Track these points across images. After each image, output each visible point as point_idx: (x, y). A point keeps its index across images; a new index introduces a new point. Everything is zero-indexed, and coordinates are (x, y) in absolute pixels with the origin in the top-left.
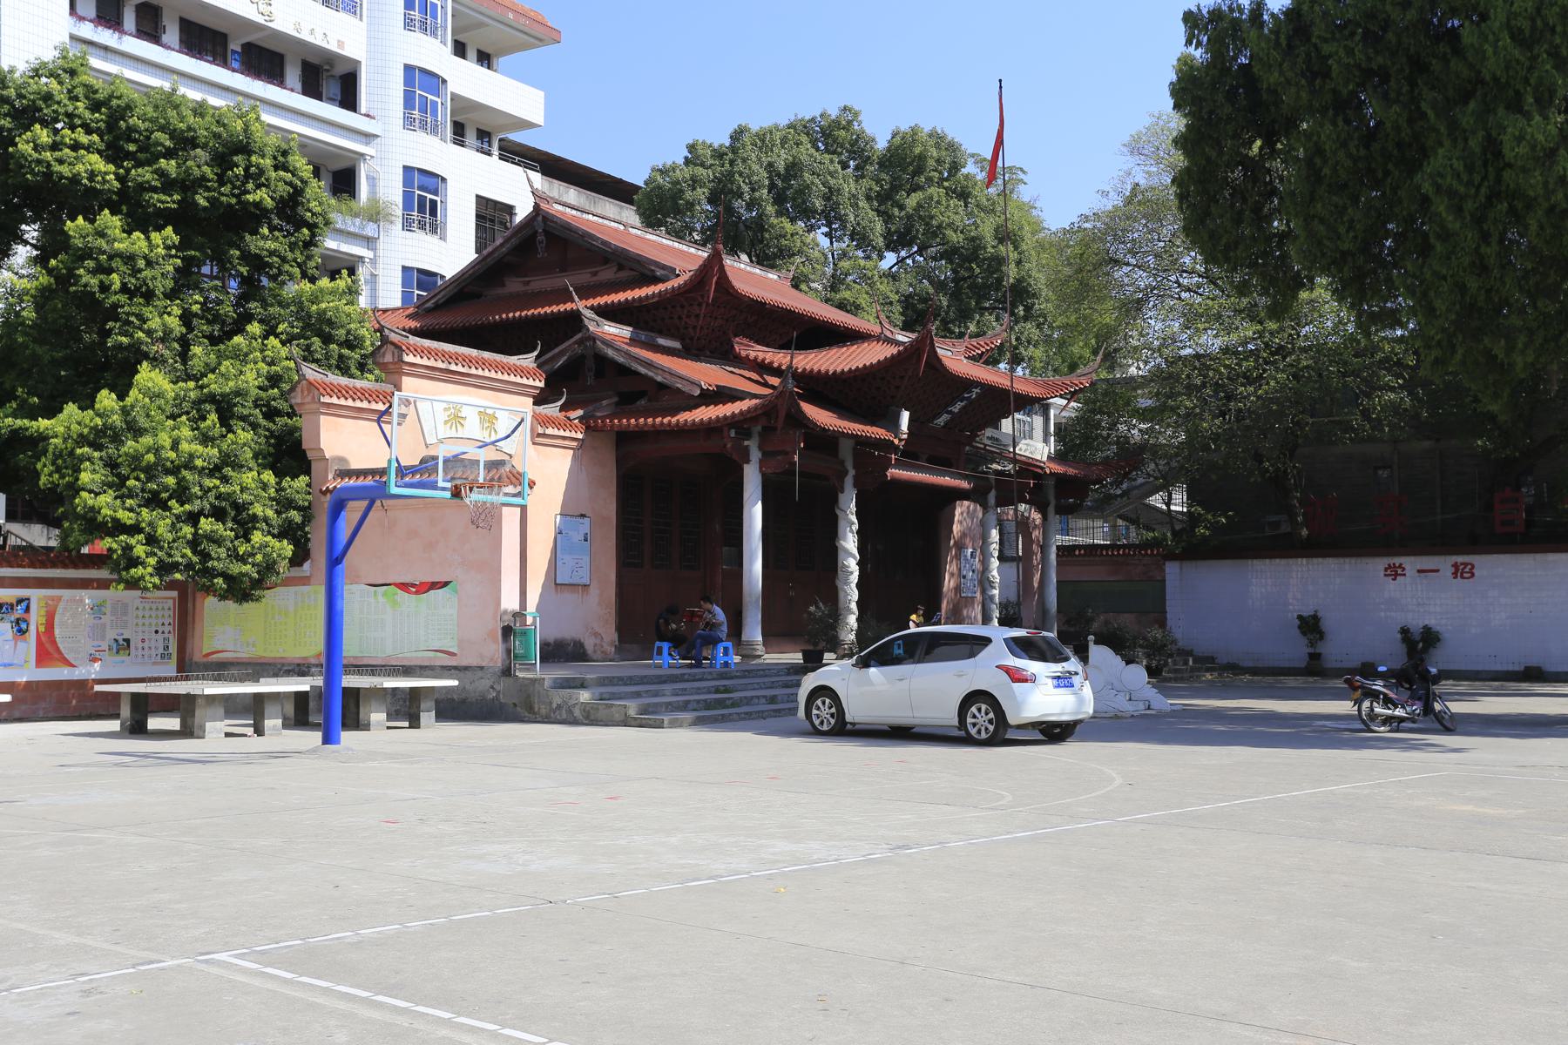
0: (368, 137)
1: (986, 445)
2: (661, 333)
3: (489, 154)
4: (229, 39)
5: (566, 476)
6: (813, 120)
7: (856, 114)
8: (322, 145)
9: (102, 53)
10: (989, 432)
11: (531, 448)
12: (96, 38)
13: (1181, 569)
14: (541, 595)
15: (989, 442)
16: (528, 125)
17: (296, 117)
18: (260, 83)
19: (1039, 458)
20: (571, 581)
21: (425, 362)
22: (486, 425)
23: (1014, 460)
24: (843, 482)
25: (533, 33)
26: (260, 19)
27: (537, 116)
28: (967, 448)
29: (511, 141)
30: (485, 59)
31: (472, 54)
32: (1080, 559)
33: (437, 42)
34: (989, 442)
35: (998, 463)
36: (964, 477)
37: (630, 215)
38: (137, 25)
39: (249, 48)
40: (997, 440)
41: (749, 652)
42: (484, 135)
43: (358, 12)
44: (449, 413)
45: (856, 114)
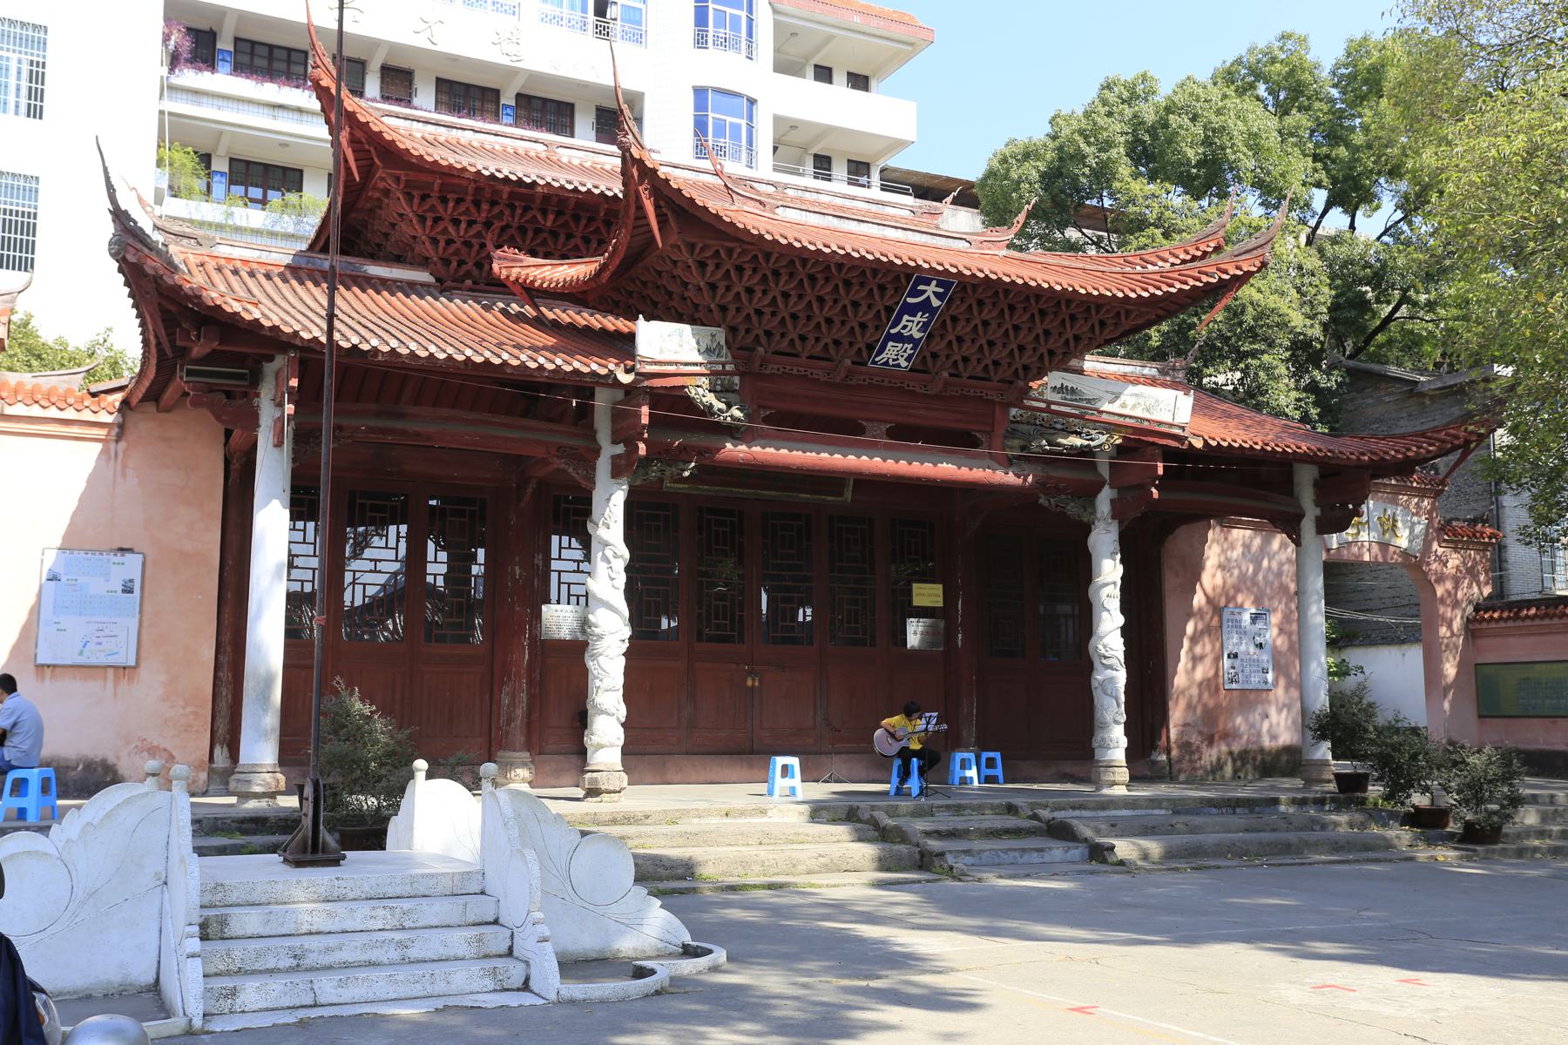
1: (1049, 403)
2: (374, 257)
4: (501, 93)
6: (1239, 61)
7: (1303, 41)
8: (214, 126)
9: (296, 115)
10: (1054, 378)
15: (1057, 397)
16: (898, 145)
18: (248, 82)
19: (1169, 420)
23: (1110, 428)
24: (594, 468)
25: (893, 35)
26: (505, 61)
27: (907, 134)
28: (1014, 411)
29: (895, 170)
30: (859, 81)
31: (840, 78)
32: (1502, 624)
34: (1057, 397)
35: (1079, 434)
36: (1008, 463)
37: (964, 220)
38: (382, 91)
40: (1073, 391)
41: (1314, 776)
42: (859, 169)
43: (517, 13)
45: (1303, 41)
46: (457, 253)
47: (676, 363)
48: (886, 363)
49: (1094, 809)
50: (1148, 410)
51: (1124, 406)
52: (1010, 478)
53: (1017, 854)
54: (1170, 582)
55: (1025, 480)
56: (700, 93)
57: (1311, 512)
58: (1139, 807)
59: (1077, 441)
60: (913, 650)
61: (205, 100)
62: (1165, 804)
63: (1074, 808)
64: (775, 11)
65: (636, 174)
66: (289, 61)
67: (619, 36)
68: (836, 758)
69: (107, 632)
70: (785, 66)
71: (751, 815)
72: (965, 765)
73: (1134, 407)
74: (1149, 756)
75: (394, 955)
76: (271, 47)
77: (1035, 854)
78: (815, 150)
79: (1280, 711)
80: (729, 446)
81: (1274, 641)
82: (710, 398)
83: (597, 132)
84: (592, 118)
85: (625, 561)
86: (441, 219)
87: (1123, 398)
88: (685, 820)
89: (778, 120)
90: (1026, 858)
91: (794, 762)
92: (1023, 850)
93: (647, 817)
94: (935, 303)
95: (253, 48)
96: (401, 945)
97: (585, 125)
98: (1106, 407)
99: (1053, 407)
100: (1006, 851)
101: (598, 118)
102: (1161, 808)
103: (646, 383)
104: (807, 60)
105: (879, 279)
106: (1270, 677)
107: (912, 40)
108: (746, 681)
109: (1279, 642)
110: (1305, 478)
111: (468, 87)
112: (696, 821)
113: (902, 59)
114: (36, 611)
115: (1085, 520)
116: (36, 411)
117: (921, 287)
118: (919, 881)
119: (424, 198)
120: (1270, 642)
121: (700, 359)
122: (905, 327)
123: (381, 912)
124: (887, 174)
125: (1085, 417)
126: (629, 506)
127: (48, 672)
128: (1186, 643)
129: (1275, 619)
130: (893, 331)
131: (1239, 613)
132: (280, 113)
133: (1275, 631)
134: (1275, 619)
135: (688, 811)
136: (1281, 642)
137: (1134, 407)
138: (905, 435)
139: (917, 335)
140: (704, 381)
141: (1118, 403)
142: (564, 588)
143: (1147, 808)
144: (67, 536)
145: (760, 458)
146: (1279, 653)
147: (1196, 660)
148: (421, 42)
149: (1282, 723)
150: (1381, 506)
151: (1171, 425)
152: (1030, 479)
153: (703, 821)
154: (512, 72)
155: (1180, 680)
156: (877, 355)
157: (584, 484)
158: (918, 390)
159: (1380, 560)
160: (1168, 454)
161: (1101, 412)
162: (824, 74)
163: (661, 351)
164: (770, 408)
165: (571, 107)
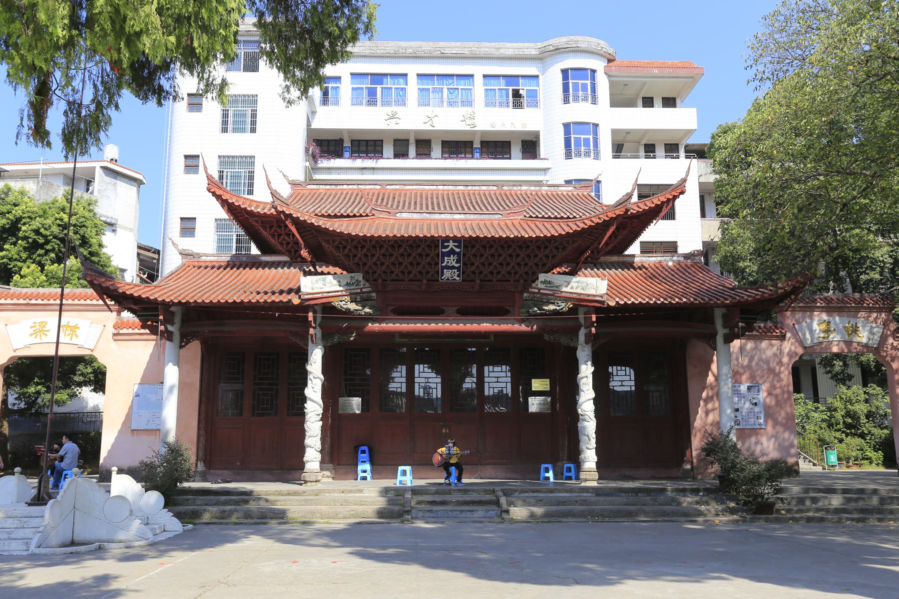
0: (545, 170)
1: (539, 289)
3: (678, 157)
5: (147, 358)
9: (372, 171)
11: (114, 345)
12: (364, 166)
13: (308, 462)
14: (117, 438)
15: (543, 286)
16: (689, 132)
17: (480, 172)
19: (595, 293)
20: (147, 428)
21: (9, 301)
22: (67, 333)
23: (566, 299)
26: (468, 128)
28: (525, 295)
30: (669, 102)
31: (658, 102)
33: (584, 104)
34: (543, 286)
36: (521, 321)
39: (483, 143)
40: (550, 282)
44: (34, 329)
46: (292, 247)
47: (321, 293)
48: (448, 279)
49: (545, 492)
50: (583, 289)
51: (572, 288)
52: (523, 328)
53: (458, 513)
54: (691, 371)
55: (532, 328)
56: (567, 126)
57: (721, 332)
58: (575, 492)
59: (552, 307)
60: (533, 413)
61: (333, 171)
62: (591, 490)
63: (533, 492)
64: (609, 76)
65: (283, 217)
66: (375, 146)
67: (525, 105)
68: (488, 467)
69: (157, 416)
70: (617, 101)
71: (355, 493)
72: (547, 471)
73: (577, 288)
74: (681, 466)
75: (6, 536)
76: (367, 141)
77: (469, 513)
78: (644, 142)
79: (769, 440)
80: (370, 324)
81: (765, 399)
82: (353, 306)
83: (523, 152)
84: (520, 146)
85: (321, 379)
86: (281, 235)
87: (571, 284)
88: (322, 494)
89: (614, 132)
90: (463, 514)
91: (408, 469)
92: (462, 511)
93: (304, 492)
94: (458, 250)
95: (367, 144)
96: (8, 533)
97: (516, 150)
98: (564, 289)
99: (541, 291)
100: (452, 511)
101: (523, 146)
102: (588, 493)
103: (307, 303)
104: (638, 95)
105: (428, 243)
106: (761, 421)
107: (692, 75)
108: (441, 430)
109: (768, 400)
110: (718, 314)
111: (457, 143)
112: (327, 495)
113: (692, 86)
114: (131, 408)
115: (572, 345)
116: (130, 331)
117: (446, 244)
118: (383, 523)
119: (271, 227)
120: (762, 401)
121: (341, 289)
122: (448, 262)
123: (16, 522)
124: (688, 148)
125: (555, 295)
126: (324, 357)
127: (136, 432)
128: (702, 403)
129: (764, 387)
130: (443, 265)
131: (739, 386)
132: (365, 171)
133: (765, 394)
134: (764, 387)
135: (324, 490)
136: (771, 401)
137: (577, 288)
138: (467, 312)
139: (457, 265)
140: (348, 298)
141: (570, 286)
142: (628, 374)
143: (579, 492)
144: (142, 379)
145: (386, 329)
146: (769, 407)
147: (707, 413)
148: (428, 127)
149: (771, 447)
150: (846, 320)
151: (595, 296)
152: (535, 327)
153: (331, 495)
154: (475, 132)
155: (698, 423)
156: (442, 276)
157: (304, 347)
158: (469, 290)
159: (846, 351)
160: (598, 310)
161: (562, 292)
162: (648, 102)
163: (313, 289)
164: (392, 305)
165: (509, 143)
